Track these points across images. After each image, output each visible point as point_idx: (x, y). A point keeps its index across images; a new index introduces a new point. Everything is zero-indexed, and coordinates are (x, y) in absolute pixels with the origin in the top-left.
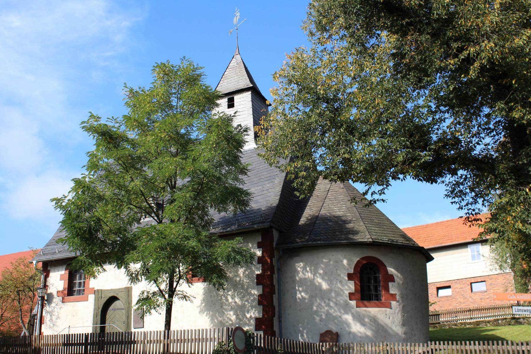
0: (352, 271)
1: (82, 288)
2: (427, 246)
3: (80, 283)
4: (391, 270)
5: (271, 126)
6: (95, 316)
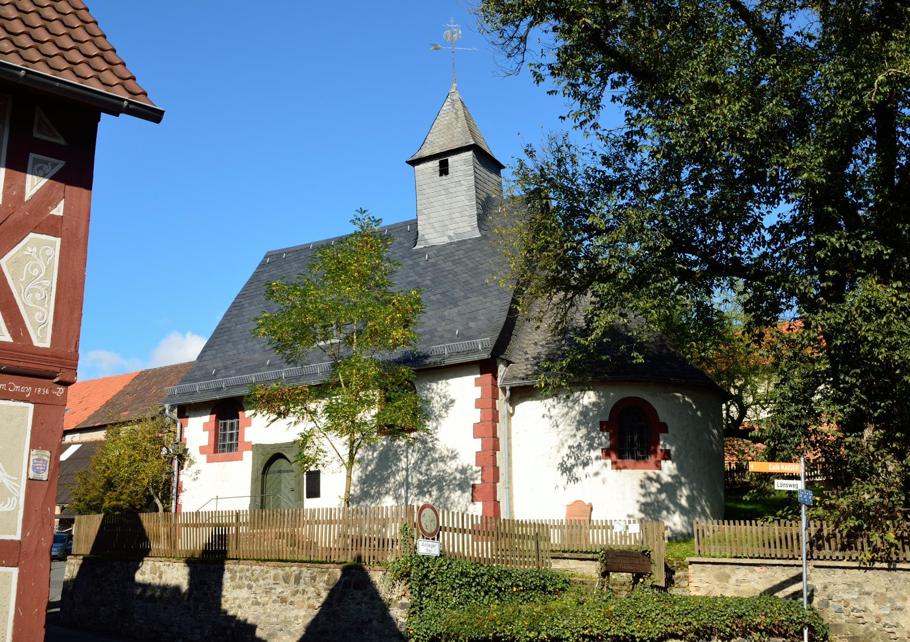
0: (606, 419)
1: (234, 442)
2: (517, 407)
3: (232, 435)
4: (663, 417)
5: (413, 310)
6: (254, 481)
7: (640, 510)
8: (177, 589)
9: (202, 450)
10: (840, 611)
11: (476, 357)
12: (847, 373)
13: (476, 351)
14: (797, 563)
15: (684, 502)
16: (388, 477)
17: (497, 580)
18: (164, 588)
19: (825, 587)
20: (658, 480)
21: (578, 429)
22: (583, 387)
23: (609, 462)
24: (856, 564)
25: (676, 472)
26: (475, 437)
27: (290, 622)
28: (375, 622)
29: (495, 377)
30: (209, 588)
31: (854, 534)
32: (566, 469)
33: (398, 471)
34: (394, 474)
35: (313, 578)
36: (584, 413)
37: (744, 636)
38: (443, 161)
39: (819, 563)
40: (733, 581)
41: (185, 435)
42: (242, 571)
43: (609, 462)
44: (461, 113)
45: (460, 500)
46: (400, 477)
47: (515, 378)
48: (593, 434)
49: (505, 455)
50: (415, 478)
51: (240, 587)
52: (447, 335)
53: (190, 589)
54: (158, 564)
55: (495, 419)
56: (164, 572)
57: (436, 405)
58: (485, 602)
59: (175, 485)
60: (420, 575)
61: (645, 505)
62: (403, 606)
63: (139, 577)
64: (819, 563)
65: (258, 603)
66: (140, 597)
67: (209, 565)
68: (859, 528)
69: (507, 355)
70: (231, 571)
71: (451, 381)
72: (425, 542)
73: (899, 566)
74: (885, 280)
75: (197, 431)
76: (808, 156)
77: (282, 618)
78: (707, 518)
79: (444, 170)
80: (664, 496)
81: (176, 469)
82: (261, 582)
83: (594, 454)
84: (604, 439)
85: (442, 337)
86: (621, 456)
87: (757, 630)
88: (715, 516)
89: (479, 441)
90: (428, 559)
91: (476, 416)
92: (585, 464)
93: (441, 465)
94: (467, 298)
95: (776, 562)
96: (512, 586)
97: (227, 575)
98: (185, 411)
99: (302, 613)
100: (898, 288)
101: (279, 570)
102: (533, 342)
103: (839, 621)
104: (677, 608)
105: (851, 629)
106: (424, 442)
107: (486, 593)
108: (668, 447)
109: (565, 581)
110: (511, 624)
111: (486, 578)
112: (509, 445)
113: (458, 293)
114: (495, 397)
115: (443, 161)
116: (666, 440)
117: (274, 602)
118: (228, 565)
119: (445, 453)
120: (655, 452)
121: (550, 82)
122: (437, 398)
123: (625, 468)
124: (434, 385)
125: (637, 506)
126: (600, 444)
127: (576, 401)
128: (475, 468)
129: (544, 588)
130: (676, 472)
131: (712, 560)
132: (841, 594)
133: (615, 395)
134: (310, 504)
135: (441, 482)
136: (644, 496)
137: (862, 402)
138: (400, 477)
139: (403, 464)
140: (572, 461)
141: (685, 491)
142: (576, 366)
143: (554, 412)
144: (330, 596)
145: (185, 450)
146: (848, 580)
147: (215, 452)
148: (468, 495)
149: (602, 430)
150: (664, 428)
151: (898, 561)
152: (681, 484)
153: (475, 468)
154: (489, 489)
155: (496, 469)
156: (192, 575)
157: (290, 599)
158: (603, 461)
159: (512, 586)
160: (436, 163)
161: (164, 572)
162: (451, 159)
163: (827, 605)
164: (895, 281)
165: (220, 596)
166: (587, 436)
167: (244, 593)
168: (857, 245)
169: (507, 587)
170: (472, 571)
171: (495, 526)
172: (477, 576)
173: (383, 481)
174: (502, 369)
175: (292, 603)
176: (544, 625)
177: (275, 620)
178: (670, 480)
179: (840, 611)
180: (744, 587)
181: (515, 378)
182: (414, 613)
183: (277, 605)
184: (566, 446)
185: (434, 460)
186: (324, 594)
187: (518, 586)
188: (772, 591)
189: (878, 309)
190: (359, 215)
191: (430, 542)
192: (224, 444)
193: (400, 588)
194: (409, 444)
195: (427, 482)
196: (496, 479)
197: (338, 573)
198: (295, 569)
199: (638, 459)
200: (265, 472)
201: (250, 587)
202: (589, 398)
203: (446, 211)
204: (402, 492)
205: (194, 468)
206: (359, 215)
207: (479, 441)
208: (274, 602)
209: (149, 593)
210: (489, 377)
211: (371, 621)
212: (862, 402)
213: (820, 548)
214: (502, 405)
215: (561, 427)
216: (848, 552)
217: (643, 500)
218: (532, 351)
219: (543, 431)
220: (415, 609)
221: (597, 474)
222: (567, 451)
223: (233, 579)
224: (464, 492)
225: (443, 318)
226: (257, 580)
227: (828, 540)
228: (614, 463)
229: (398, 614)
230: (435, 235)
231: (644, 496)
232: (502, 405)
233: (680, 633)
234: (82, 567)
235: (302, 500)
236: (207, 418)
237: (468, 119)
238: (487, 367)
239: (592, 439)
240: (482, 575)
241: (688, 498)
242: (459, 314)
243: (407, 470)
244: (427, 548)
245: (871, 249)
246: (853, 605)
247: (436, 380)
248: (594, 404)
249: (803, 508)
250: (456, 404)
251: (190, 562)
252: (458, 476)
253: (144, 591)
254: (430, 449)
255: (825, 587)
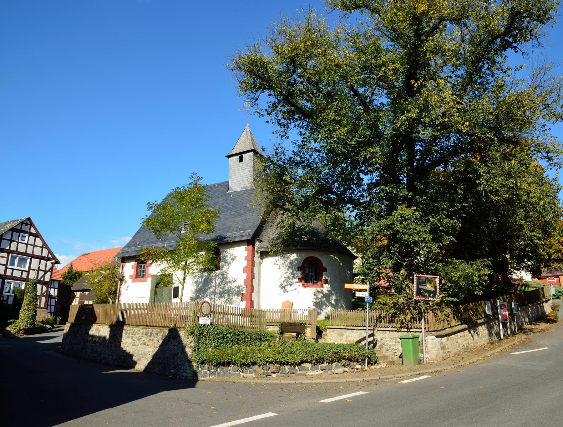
0: (300, 265)
4: (325, 265)
6: (151, 290)
7: (314, 305)
8: (105, 338)
9: (131, 277)
10: (387, 350)
11: (245, 238)
12: (393, 246)
13: (246, 236)
14: (420, 330)
15: (333, 302)
16: (207, 290)
17: (238, 336)
18: (100, 337)
19: (382, 339)
20: (322, 292)
21: (288, 270)
22: (291, 251)
23: (301, 284)
24: (394, 329)
25: (330, 289)
26: (244, 272)
27: (146, 354)
28: (179, 354)
29: (254, 247)
30: (117, 338)
31: (394, 316)
32: (283, 287)
33: (211, 287)
34: (210, 288)
35: (157, 334)
36: (291, 263)
37: (338, 362)
38: (240, 156)
39: (379, 329)
40: (345, 336)
41: (124, 271)
42: (130, 330)
43: (301, 284)
44: (249, 136)
45: (237, 299)
46: (212, 290)
47: (262, 247)
48: (295, 272)
49: (257, 281)
50: (219, 290)
51: (129, 338)
52: (235, 229)
53: (110, 338)
54: (99, 327)
55: (253, 264)
56: (100, 330)
57: (229, 259)
58: (230, 345)
59: (118, 292)
60: (200, 334)
61: (316, 303)
62: (191, 347)
63: (91, 332)
64: (379, 329)
65: (135, 345)
66: (90, 341)
67: (117, 328)
68: (396, 313)
69: (260, 237)
70: (126, 330)
71: (235, 248)
72: (204, 318)
73: (411, 330)
74: (409, 206)
75: (129, 268)
76: (377, 153)
77: (143, 351)
78: (343, 309)
79: (241, 160)
80: (324, 299)
81: (119, 285)
82: (137, 335)
83: (295, 281)
84: (299, 274)
85: (233, 230)
86: (306, 282)
87: (344, 358)
88: (348, 308)
89: (246, 274)
90: (204, 326)
91: (245, 263)
92: (291, 285)
93: (229, 285)
94: (245, 213)
95: (359, 328)
96: (245, 338)
97: (124, 332)
98: (124, 260)
99: (152, 350)
100: (414, 210)
101: (144, 330)
102: (271, 234)
103: (387, 354)
104: (309, 349)
105: (392, 358)
106: (223, 274)
107: (232, 341)
108: (327, 278)
109: (271, 336)
110: (235, 355)
111: (231, 335)
112: (259, 276)
113: (242, 211)
114: (253, 255)
115: (240, 156)
116: (326, 275)
117: (141, 344)
118: (125, 328)
119: (231, 279)
120: (321, 280)
121: (267, 117)
122: (229, 256)
123: (308, 287)
124: (228, 250)
125: (312, 303)
126: (298, 277)
127: (288, 258)
128: (244, 286)
129: (261, 339)
130: (330, 289)
131: (337, 327)
132: (388, 342)
133: (304, 255)
134: (174, 301)
135: (229, 292)
136: (316, 299)
137: (399, 258)
138: (212, 290)
139: (214, 284)
140: (285, 284)
141: (334, 297)
142: (288, 243)
143: (279, 262)
144: (163, 342)
145: (123, 277)
146: (391, 336)
147: (136, 277)
148: (240, 298)
149: (298, 270)
150: (325, 270)
151: (411, 328)
152: (332, 294)
153: (244, 286)
154: (249, 295)
155: (252, 287)
156: (111, 332)
157: (147, 343)
158: (298, 284)
159: (245, 338)
160: (238, 157)
161: (100, 330)
162: (244, 155)
163: (382, 347)
164: (414, 206)
165: (121, 341)
166: (292, 273)
167: (130, 340)
168: (397, 191)
169: (242, 338)
170: (224, 331)
171: (250, 312)
172: (227, 333)
173: (205, 291)
174: (257, 244)
175: (148, 345)
176: (249, 356)
177: (141, 352)
178: (327, 292)
179: (387, 350)
180: (349, 339)
181: (262, 247)
182: (195, 350)
183: (142, 346)
184: (283, 277)
185: (227, 282)
186: (161, 341)
187: (248, 338)
188: (359, 341)
189: (405, 218)
190: (193, 175)
191: (206, 318)
192: (140, 275)
193: (191, 338)
194: (216, 276)
195: (223, 292)
196: (252, 291)
197: (167, 332)
198: (150, 329)
199: (314, 283)
200: (156, 287)
201: (132, 338)
202: (294, 256)
203: (241, 177)
204: (213, 296)
205: (127, 285)
206: (193, 175)
207: (246, 274)
208: (141, 344)
209: (94, 339)
210: (251, 247)
211: (178, 353)
212: (399, 258)
213: (380, 322)
214: (257, 259)
215: (281, 269)
216: (391, 324)
217: (315, 301)
218: (271, 237)
219: (275, 272)
220: (196, 349)
221: (296, 289)
222: (284, 279)
223: (126, 334)
224: (238, 296)
225: (235, 222)
226: (135, 334)
227: (384, 319)
228: (303, 285)
229: (189, 350)
230: (236, 187)
231: (316, 299)
232: (257, 259)
233: (309, 360)
234: (70, 327)
235: (171, 299)
236: (133, 263)
237: (252, 139)
238: (251, 242)
239: (294, 274)
240: (230, 333)
241: (335, 300)
242: (242, 220)
243: (215, 287)
244: (204, 321)
245: (404, 192)
246: (393, 347)
247: (229, 248)
248: (295, 259)
249: (368, 304)
250: (237, 258)
251: (110, 326)
252: (236, 289)
253: (92, 339)
254: (225, 278)
255: (382, 339)
